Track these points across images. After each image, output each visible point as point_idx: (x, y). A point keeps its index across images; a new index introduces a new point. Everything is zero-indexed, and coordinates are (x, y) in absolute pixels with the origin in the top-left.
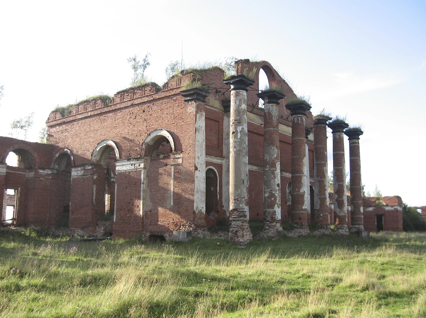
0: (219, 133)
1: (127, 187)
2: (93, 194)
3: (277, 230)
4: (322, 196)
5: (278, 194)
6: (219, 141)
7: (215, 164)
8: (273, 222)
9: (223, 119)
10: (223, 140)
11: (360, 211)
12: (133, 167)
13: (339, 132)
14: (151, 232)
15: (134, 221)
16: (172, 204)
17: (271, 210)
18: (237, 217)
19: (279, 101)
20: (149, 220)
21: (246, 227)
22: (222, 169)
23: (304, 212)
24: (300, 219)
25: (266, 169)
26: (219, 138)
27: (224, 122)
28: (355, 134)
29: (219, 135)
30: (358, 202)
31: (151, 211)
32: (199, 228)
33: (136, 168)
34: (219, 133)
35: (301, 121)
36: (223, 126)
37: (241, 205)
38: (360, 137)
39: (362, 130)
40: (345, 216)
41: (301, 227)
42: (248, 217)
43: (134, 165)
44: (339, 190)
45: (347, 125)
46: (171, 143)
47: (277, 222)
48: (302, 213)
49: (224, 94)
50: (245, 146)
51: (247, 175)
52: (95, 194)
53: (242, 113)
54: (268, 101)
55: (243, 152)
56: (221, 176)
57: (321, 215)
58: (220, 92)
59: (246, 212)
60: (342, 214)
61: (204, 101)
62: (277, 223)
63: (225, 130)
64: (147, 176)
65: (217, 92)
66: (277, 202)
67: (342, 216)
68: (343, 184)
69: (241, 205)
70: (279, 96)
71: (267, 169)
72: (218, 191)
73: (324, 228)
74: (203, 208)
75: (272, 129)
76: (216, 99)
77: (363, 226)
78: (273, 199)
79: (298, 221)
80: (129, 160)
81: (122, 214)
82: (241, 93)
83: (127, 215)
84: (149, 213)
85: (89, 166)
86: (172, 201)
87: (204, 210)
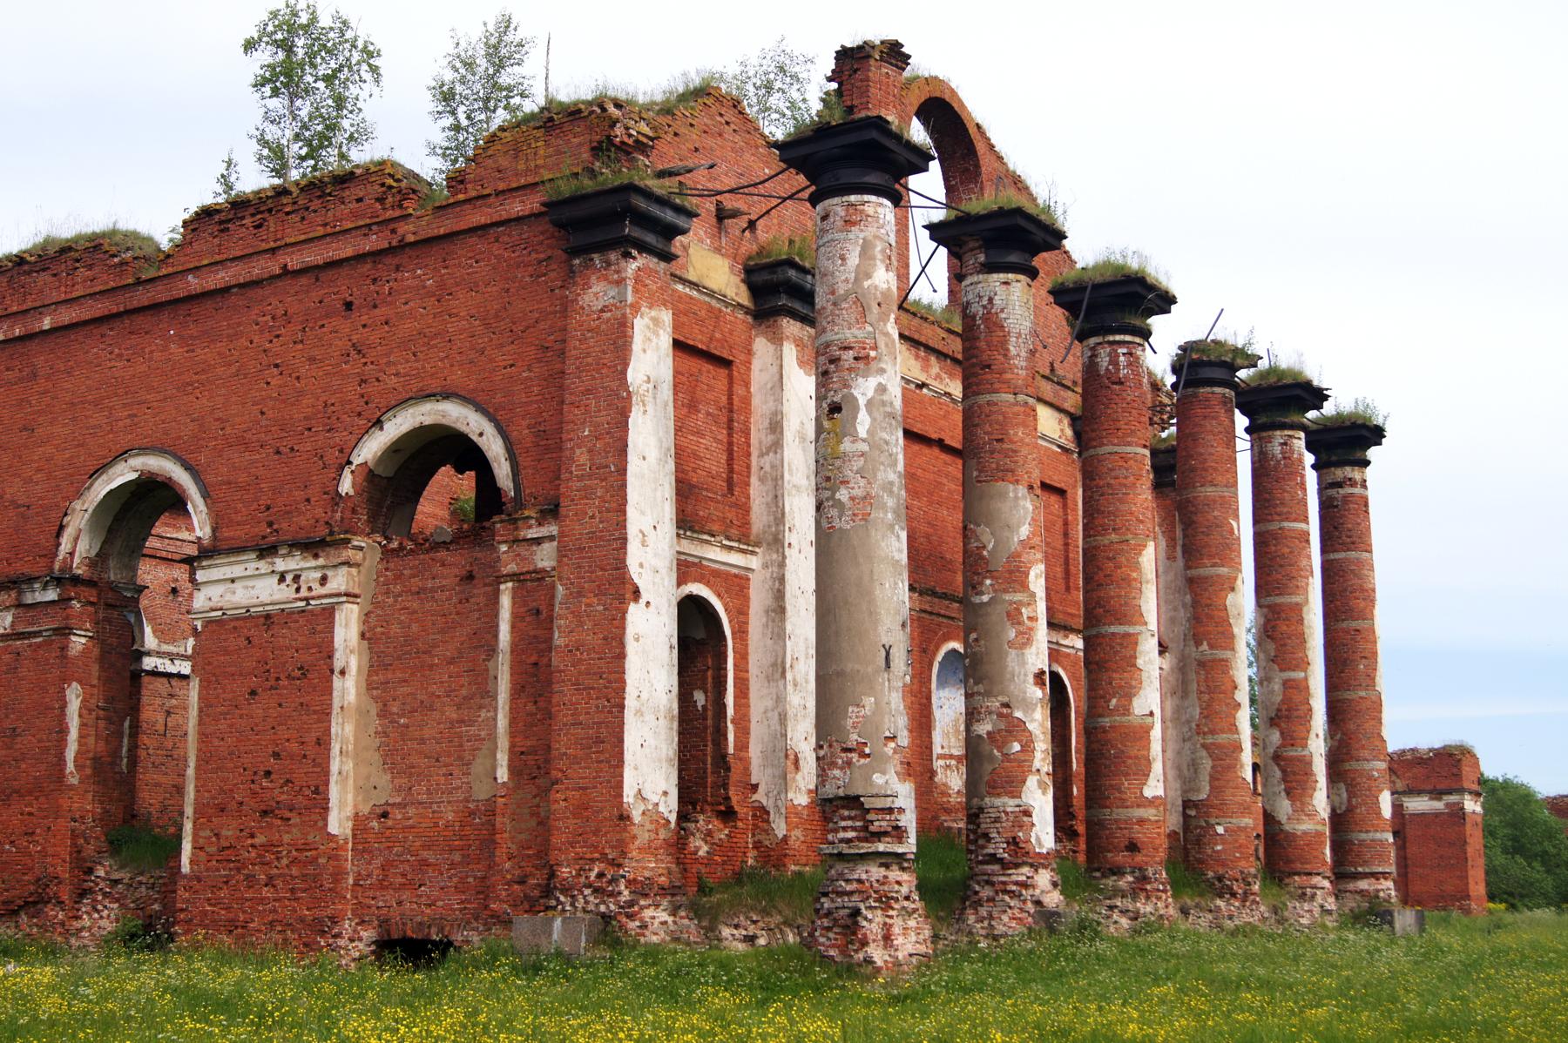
0: (731, 421)
1: (253, 693)
2: (63, 731)
3: (1038, 903)
4: (1222, 738)
5: (1042, 725)
6: (730, 459)
7: (716, 574)
8: (1017, 866)
9: (750, 353)
10: (749, 455)
11: (1378, 813)
12: (284, 593)
13: (1283, 426)
14: (384, 923)
15: (294, 871)
16: (503, 774)
17: (1010, 804)
18: (859, 839)
19: (1037, 262)
20: (378, 862)
21: (904, 890)
22: (747, 599)
23: (1150, 813)
24: (1133, 847)
25: (977, 600)
26: (730, 444)
27: (756, 365)
28: (1349, 441)
29: (730, 428)
30: (1367, 766)
31: (385, 815)
32: (646, 896)
33: (304, 593)
34: (731, 421)
35: (1130, 364)
36: (747, 385)
37: (878, 779)
38: (1373, 453)
39: (1379, 421)
40: (1319, 834)
41: (1141, 886)
42: (913, 839)
43: (297, 578)
44: (1282, 717)
45: (1317, 396)
46: (495, 466)
47: (1038, 862)
48: (1141, 821)
49: (752, 225)
50: (892, 477)
51: (903, 625)
52: (73, 734)
53: (875, 309)
54: (982, 258)
55: (883, 507)
56: (741, 632)
57: (1220, 830)
58: (735, 214)
59: (901, 810)
60: (1305, 826)
61: (668, 257)
62: (1035, 867)
63: (760, 405)
64: (363, 636)
65: (722, 215)
66: (1037, 764)
67: (1305, 833)
68: (1306, 679)
69: (878, 779)
70: (1040, 235)
71: (985, 598)
72: (730, 712)
73: (1234, 895)
74: (1151, 714)
75: (1010, 397)
76: (718, 250)
77: (1390, 884)
78: (1016, 747)
79: (1121, 858)
80: (266, 551)
81: (224, 832)
82: (870, 210)
83: (252, 836)
84: (375, 824)
85: (45, 588)
86: (503, 758)
87: (669, 807)
